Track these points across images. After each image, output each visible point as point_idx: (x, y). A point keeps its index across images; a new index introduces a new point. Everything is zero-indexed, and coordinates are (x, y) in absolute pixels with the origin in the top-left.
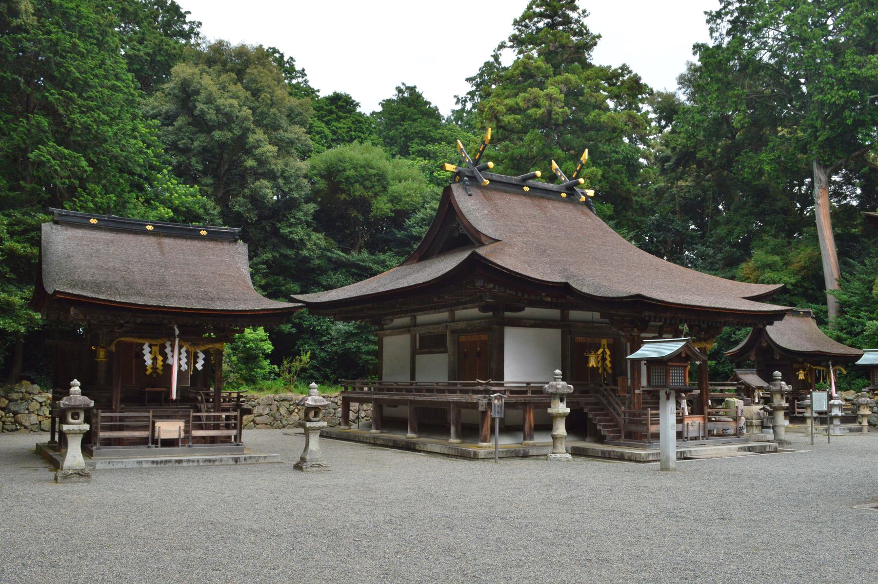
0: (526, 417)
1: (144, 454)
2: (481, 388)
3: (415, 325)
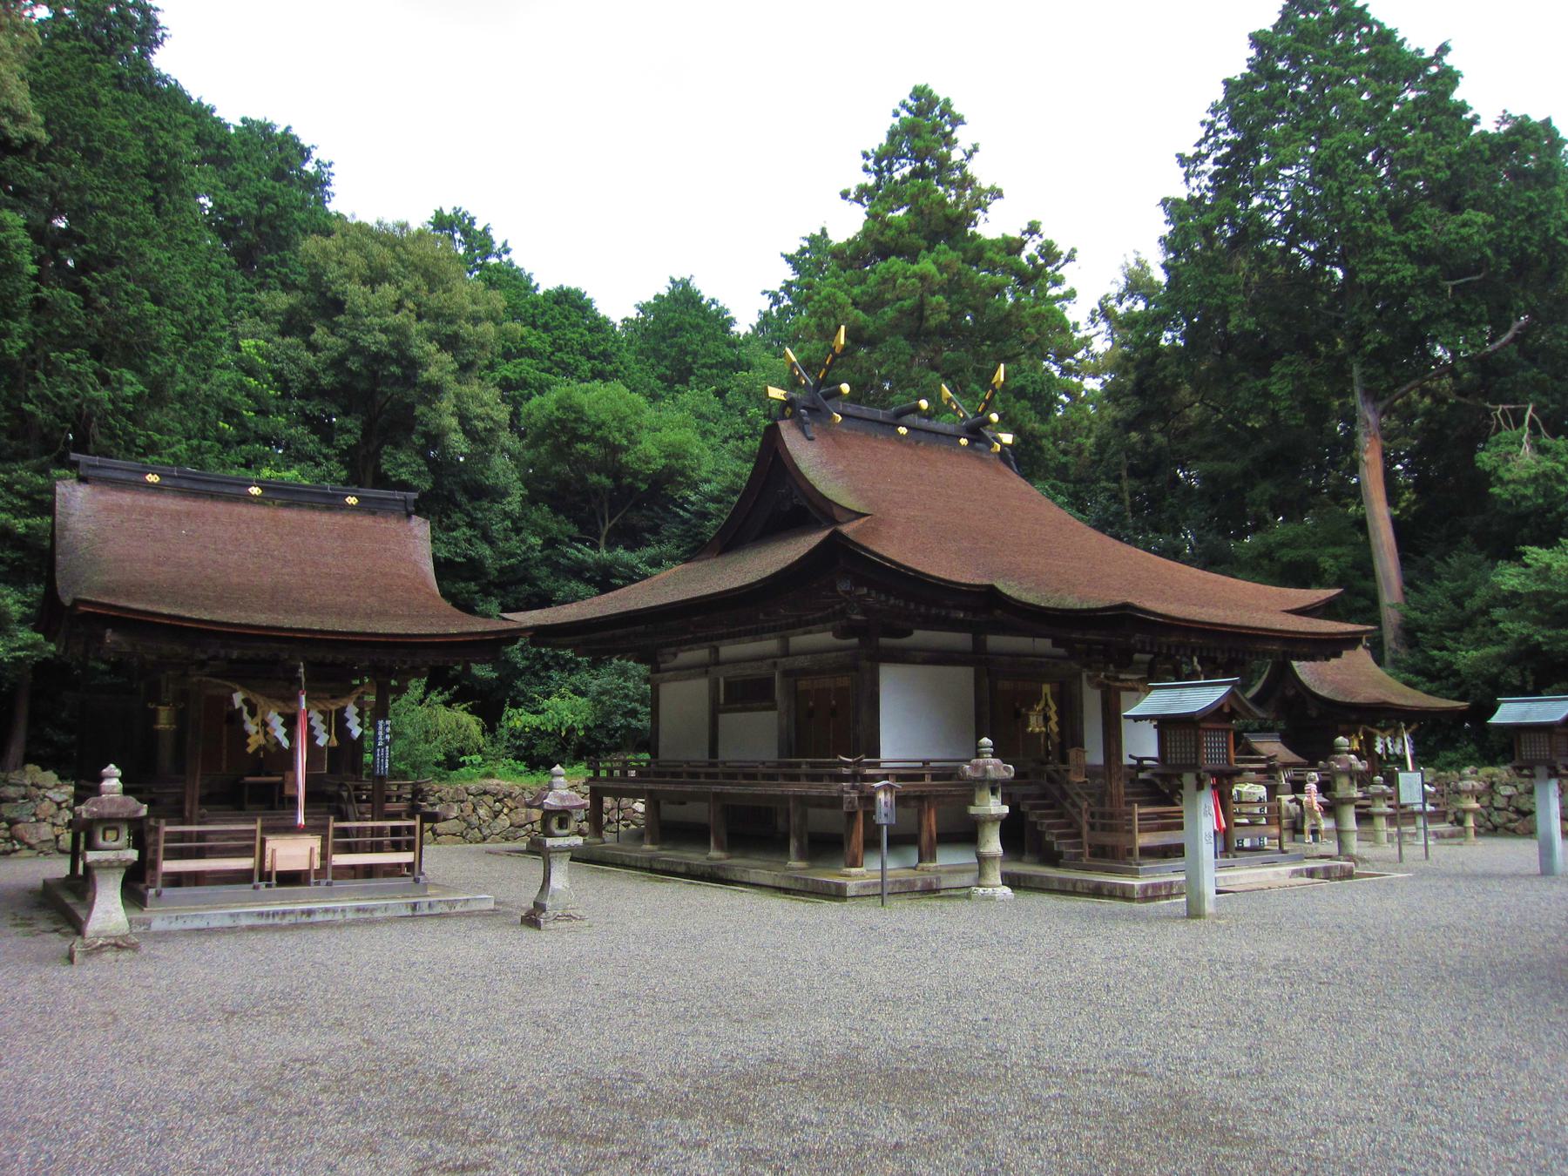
0: (936, 817)
1: (242, 902)
2: (846, 771)
3: (717, 663)
